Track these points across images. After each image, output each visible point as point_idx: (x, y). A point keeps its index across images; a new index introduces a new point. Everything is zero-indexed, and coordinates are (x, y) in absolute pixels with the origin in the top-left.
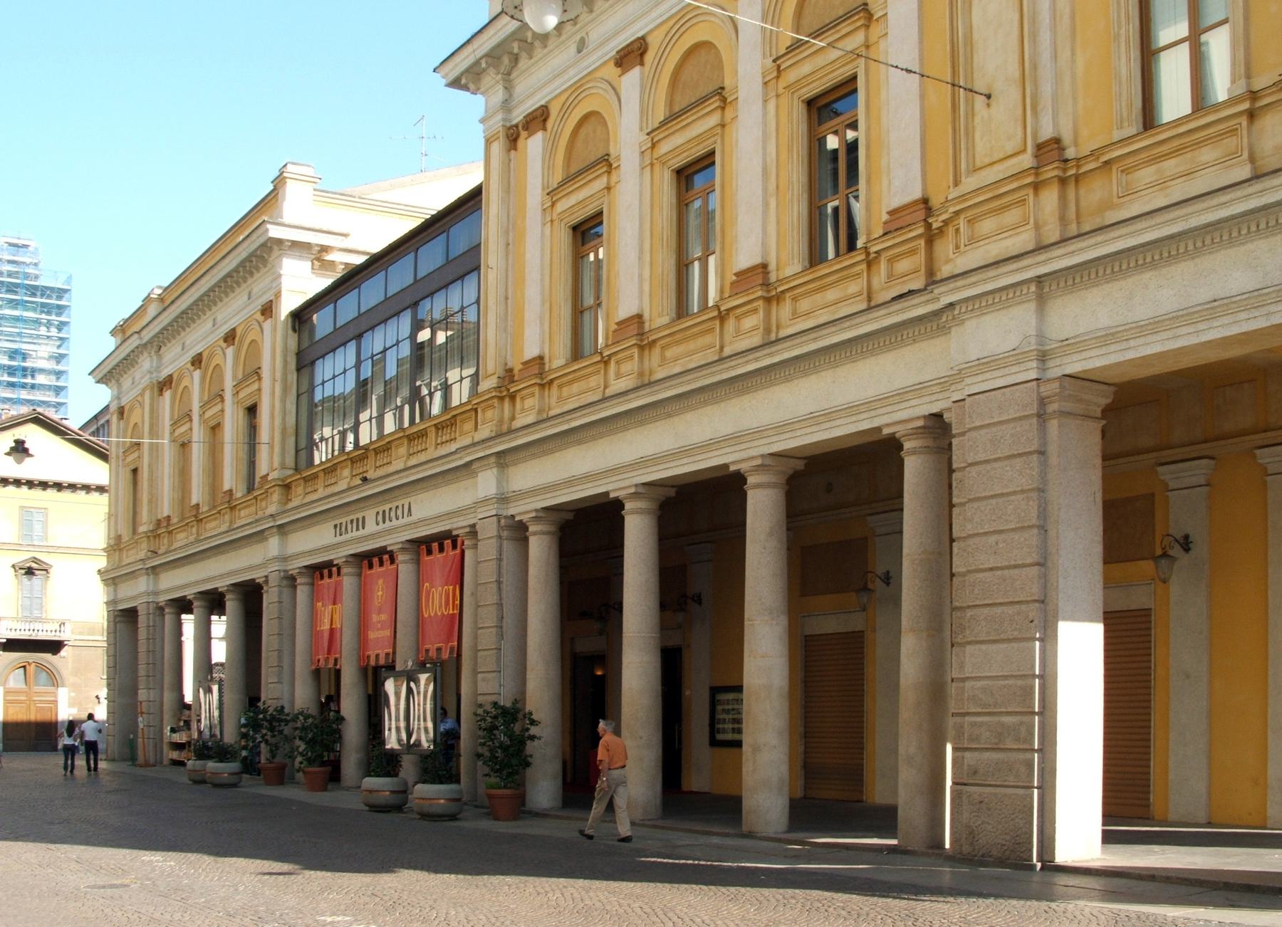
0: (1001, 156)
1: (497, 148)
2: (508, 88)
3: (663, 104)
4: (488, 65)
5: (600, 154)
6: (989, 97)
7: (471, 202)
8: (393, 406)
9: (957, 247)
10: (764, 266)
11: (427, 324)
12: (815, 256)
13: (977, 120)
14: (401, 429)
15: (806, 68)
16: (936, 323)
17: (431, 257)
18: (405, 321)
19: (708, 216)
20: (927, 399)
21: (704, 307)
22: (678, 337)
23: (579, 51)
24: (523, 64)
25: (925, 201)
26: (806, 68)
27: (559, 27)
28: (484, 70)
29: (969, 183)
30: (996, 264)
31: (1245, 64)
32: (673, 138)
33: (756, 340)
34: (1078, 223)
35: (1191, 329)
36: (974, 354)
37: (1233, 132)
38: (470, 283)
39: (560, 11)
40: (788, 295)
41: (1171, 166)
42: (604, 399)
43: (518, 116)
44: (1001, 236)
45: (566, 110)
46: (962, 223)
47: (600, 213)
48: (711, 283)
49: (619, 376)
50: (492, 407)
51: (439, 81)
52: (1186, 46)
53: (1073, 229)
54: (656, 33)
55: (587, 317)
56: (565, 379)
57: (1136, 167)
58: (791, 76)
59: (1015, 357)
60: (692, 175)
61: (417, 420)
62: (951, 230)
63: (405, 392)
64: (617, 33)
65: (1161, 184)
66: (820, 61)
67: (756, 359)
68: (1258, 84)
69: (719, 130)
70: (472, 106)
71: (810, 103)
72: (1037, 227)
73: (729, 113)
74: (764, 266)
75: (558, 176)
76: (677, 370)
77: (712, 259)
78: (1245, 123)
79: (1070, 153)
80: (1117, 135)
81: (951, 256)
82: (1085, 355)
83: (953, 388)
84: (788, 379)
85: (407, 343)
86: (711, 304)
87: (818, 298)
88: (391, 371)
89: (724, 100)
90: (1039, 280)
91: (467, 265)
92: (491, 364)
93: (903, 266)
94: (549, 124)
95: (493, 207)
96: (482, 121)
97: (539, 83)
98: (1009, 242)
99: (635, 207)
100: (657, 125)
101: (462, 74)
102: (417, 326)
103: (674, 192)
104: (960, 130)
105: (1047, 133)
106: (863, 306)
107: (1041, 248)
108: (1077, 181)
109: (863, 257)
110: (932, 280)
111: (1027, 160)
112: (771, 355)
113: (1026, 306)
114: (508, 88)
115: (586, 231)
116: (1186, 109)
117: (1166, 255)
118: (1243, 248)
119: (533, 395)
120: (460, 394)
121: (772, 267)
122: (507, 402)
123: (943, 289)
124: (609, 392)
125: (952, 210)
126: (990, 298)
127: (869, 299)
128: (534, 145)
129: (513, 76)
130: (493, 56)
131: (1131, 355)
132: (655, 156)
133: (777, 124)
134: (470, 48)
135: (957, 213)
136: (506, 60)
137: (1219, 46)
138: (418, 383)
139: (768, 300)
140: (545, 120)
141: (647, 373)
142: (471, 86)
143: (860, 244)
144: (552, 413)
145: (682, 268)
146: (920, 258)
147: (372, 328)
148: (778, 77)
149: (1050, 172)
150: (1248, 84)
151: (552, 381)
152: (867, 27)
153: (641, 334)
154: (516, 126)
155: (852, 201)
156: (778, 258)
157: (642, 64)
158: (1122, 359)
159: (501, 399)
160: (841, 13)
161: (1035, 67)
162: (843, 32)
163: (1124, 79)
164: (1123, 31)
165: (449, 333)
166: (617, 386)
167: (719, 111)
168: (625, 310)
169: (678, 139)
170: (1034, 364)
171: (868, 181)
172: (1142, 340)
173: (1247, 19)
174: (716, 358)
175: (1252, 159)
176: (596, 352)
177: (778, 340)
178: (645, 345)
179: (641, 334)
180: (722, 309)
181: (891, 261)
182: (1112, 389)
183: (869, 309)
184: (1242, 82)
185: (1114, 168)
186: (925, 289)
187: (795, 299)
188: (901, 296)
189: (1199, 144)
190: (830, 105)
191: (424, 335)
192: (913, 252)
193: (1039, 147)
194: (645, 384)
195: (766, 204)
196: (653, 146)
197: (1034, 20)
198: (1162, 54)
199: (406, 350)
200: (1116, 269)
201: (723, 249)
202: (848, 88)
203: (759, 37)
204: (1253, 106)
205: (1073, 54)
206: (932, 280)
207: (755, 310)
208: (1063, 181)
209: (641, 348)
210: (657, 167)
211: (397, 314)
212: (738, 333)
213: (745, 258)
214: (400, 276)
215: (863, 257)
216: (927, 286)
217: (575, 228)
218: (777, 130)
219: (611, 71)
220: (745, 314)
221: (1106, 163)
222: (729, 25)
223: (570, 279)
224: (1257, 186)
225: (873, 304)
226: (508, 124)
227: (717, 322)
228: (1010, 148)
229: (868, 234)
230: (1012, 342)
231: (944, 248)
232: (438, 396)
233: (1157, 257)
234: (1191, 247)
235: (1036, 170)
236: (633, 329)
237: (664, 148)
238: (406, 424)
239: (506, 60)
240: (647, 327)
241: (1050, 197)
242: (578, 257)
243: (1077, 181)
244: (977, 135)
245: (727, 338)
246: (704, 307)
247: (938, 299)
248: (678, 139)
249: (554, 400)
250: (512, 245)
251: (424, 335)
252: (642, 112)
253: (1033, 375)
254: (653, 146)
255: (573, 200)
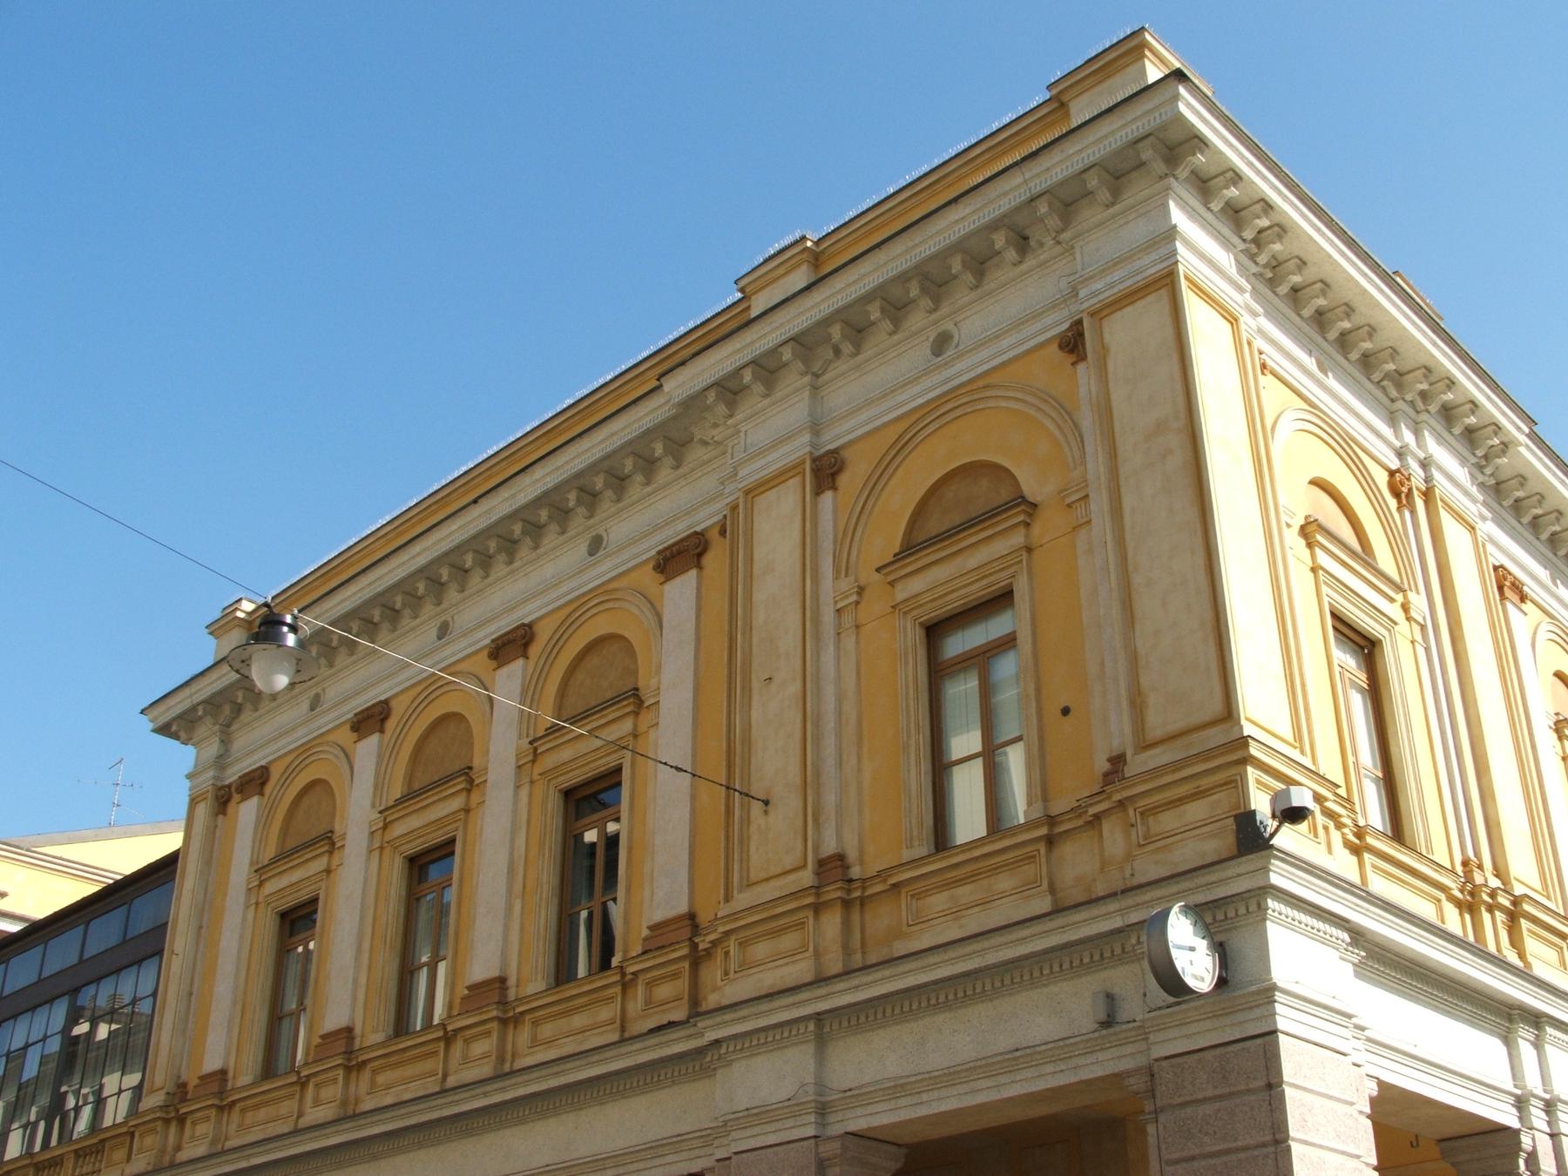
0: (779, 870)
1: (202, 810)
2: (226, 741)
3: (401, 777)
4: (205, 713)
5: (321, 829)
6: (766, 803)
7: (164, 870)
8: (24, 1121)
9: (726, 973)
10: (502, 981)
11: (88, 1013)
12: (563, 972)
13: (753, 828)
14: (29, 1153)
15: (566, 754)
16: (700, 1062)
17: (104, 934)
18: (60, 1012)
19: (443, 910)
20: (685, 1155)
21: (428, 1024)
22: (393, 1059)
23: (312, 709)
24: (246, 716)
25: (691, 916)
26: (566, 754)
27: (292, 685)
28: (201, 718)
29: (742, 900)
30: (770, 996)
31: (1041, 788)
32: (407, 820)
33: (486, 1070)
34: (864, 953)
35: (990, 1083)
36: (742, 1102)
37: (1031, 858)
38: (147, 974)
39: (292, 671)
40: (528, 1017)
41: (965, 893)
42: (296, 1132)
43: (232, 775)
44: (775, 965)
45: (290, 774)
46: (732, 946)
47: (315, 900)
48: (438, 995)
49: (317, 1103)
50: (154, 1130)
51: (146, 724)
52: (979, 762)
53: (857, 960)
54: (401, 698)
55: (286, 1025)
56: (249, 1102)
57: (927, 893)
58: (549, 761)
59: (790, 1108)
60: (428, 865)
61: (54, 1142)
62: (719, 953)
63: (44, 1100)
64: (357, 693)
65: (955, 913)
66: (582, 747)
67: (485, 1095)
68: (1059, 806)
69: (462, 816)
70: (181, 757)
71: (568, 794)
72: (817, 955)
73: (475, 797)
74: (502, 981)
75: (270, 852)
76: (389, 1100)
77: (442, 968)
78: (1043, 850)
79: (855, 872)
80: (907, 855)
81: (719, 983)
82: (870, 1109)
83: (717, 1143)
84: (522, 1121)
85: (58, 1039)
86: (436, 1021)
87: (563, 1023)
88: (31, 1070)
89: (471, 781)
90: (818, 1017)
91: (148, 947)
92: (160, 1076)
93: (664, 991)
94: (268, 789)
95: (189, 880)
96: (190, 776)
97: (256, 743)
98: (786, 971)
99: (357, 894)
100: (391, 803)
101: (174, 719)
102: (73, 1018)
103: (404, 884)
104: (734, 840)
105: (830, 847)
106: (615, 1037)
107: (821, 980)
108: (862, 905)
109: (618, 978)
110: (696, 1011)
111: (807, 877)
112: (503, 1089)
113: (803, 1047)
114: (226, 741)
115: (298, 920)
116: (981, 831)
117: (961, 994)
118: (1045, 990)
119: (208, 1119)
120: (116, 1111)
121: (512, 982)
122: (173, 1129)
123: (708, 1022)
124: (303, 1123)
125: (721, 929)
126: (762, 1035)
127: (623, 1029)
128: (247, 811)
129: (233, 728)
130: (213, 704)
131: (923, 1111)
132: (387, 838)
133: (529, 815)
134: (187, 692)
135: (727, 934)
136: (227, 710)
137: (1015, 761)
138: (64, 1089)
139: (504, 1022)
140: (263, 784)
141: (352, 1100)
142: (183, 735)
143: (615, 962)
144: (230, 1144)
145: (406, 974)
146: (683, 984)
147: (15, 1016)
148: (533, 761)
149: (833, 892)
150: (1045, 808)
151: (234, 1103)
152: (636, 714)
153: (349, 1053)
154: (229, 786)
155: (611, 904)
156: (519, 969)
157: (382, 731)
158: (914, 1116)
159: (167, 1121)
160: (609, 695)
161: (818, 774)
162: (610, 717)
163: (914, 792)
164: (912, 742)
165: (114, 1027)
166: (314, 1115)
167: (464, 794)
168: (333, 1020)
169: (415, 822)
170: (812, 1118)
171: (628, 889)
172: (936, 1094)
173: (1041, 738)
174: (437, 1089)
175: (1052, 890)
176: (292, 1070)
177: (512, 1073)
178: (353, 1066)
179: (349, 1053)
180: (449, 1028)
181: (650, 984)
182: (903, 1151)
183: (622, 1041)
184: (1039, 805)
185: (904, 891)
186: (687, 1021)
187: (536, 1023)
188: (659, 1028)
189: (995, 870)
190: (591, 796)
191: (82, 1028)
192: (675, 976)
193: (821, 863)
194: (348, 1116)
195: (509, 908)
196: (385, 827)
197: (817, 725)
198: (956, 769)
199: (54, 1045)
200: (906, 1008)
201: (456, 952)
202: (612, 778)
203: (516, 715)
204: (1051, 831)
205: (859, 760)
206: (696, 1011)
207: (488, 1033)
208: (847, 904)
209: (348, 1070)
210: (387, 852)
211: (51, 1001)
212: (466, 1060)
213: (481, 969)
214: (62, 954)
215: (618, 978)
216: (690, 1017)
217: (283, 915)
218: (529, 822)
219: (345, 736)
220: (475, 1038)
221: (894, 885)
222: (486, 701)
223: (270, 979)
224: (1058, 921)
225: (627, 1035)
226: (220, 784)
227: (442, 1044)
228: (789, 861)
229: (625, 952)
230: (786, 1090)
231: (712, 973)
232: (87, 1111)
233: (951, 997)
234: (988, 987)
235: (817, 889)
236: (340, 1046)
237: (398, 830)
238: (37, 1148)
239: (227, 710)
240: (357, 1044)
241: (832, 922)
242: (283, 951)
243: (862, 905)
244: (753, 849)
245: (454, 1063)
246: (428, 1024)
247: (702, 1035)
248: (415, 822)
249: (233, 1127)
250: (206, 929)
251: (82, 1028)
252: (376, 787)
253: (810, 1131)
254: (385, 827)
255: (284, 881)
